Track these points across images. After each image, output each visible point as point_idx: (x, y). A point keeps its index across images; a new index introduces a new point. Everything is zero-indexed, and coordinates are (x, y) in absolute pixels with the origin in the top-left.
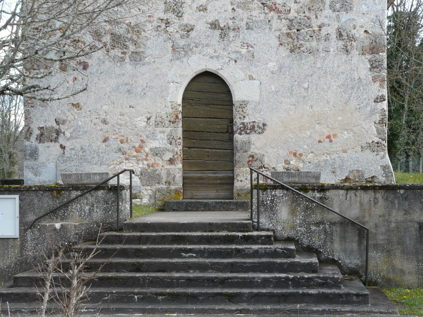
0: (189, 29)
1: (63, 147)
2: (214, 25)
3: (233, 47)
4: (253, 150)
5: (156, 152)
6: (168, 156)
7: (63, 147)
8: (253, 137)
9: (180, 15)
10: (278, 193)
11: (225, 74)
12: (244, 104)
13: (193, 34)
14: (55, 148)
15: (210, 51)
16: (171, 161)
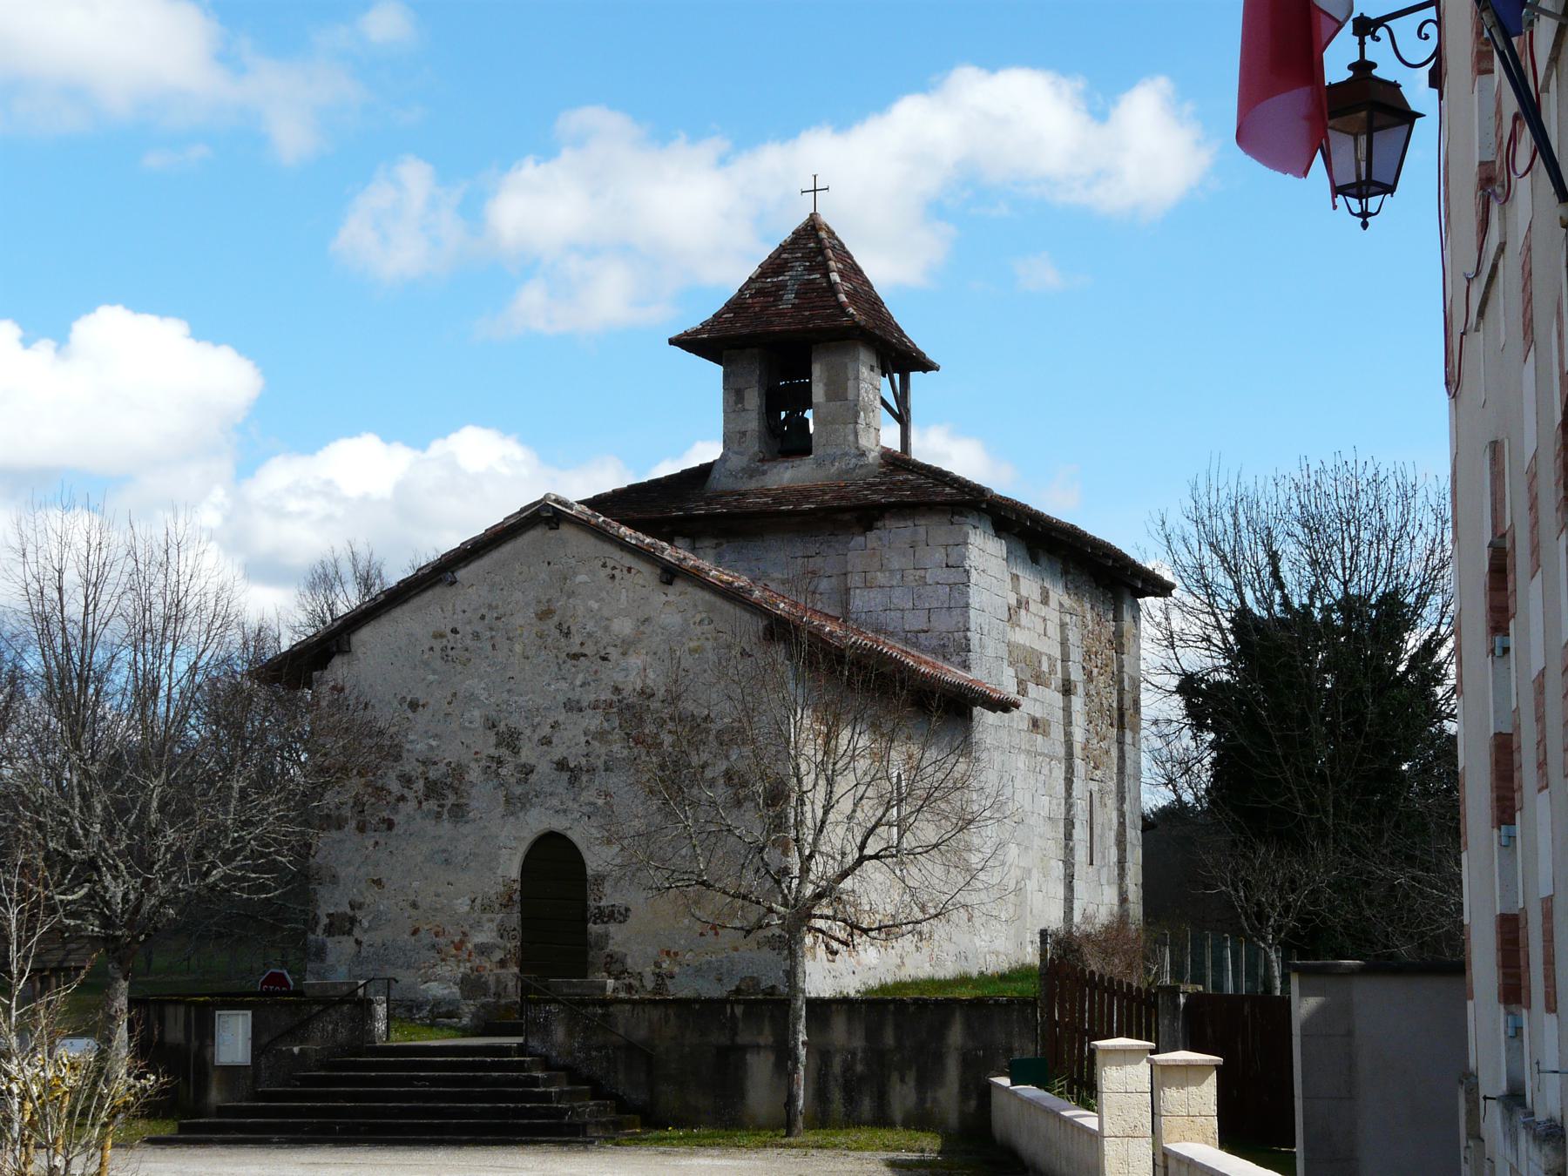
0: (527, 770)
1: (358, 942)
2: (561, 765)
3: (586, 796)
4: (612, 947)
5: (483, 950)
6: (498, 955)
7: (358, 942)
8: (612, 928)
9: (516, 751)
10: (553, 1008)
11: (575, 836)
12: (600, 879)
13: (533, 778)
14: (347, 944)
15: (555, 802)
16: (502, 963)
